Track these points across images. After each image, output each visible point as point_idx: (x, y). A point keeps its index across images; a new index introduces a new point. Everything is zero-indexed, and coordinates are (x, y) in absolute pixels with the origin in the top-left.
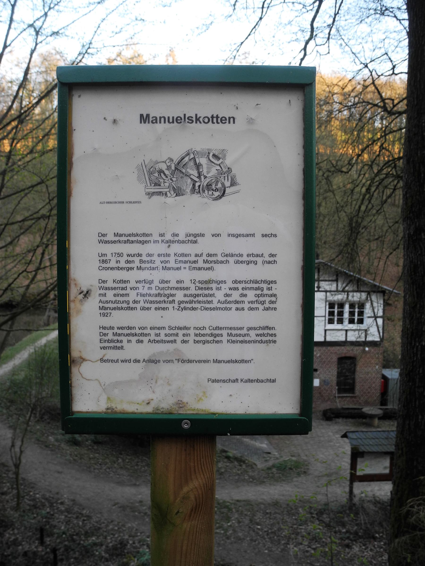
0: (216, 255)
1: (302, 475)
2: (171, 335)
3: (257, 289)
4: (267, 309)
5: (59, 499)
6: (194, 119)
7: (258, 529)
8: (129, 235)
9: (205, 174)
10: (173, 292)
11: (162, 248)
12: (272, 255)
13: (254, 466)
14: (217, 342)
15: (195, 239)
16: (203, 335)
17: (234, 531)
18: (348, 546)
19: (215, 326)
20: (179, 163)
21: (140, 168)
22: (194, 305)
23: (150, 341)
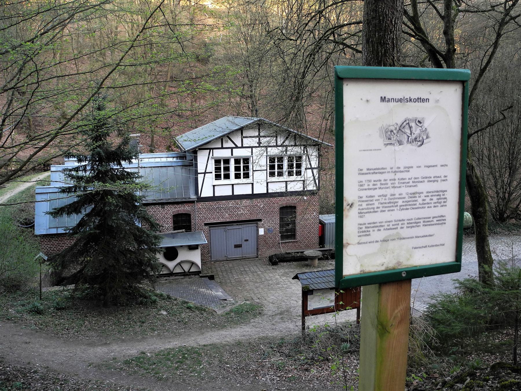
0: (418, 178)
1: (258, 316)
2: (395, 225)
3: (438, 195)
4: (442, 206)
5: (31, 368)
6: (409, 100)
7: (227, 367)
8: (375, 169)
9: (414, 132)
10: (397, 200)
11: (391, 176)
12: (445, 176)
13: (214, 313)
14: (418, 226)
15: (408, 170)
16: (411, 223)
17: (207, 372)
18: (307, 370)
19: (417, 218)
20: (401, 126)
21: (381, 129)
22: (407, 207)
23: (384, 229)
